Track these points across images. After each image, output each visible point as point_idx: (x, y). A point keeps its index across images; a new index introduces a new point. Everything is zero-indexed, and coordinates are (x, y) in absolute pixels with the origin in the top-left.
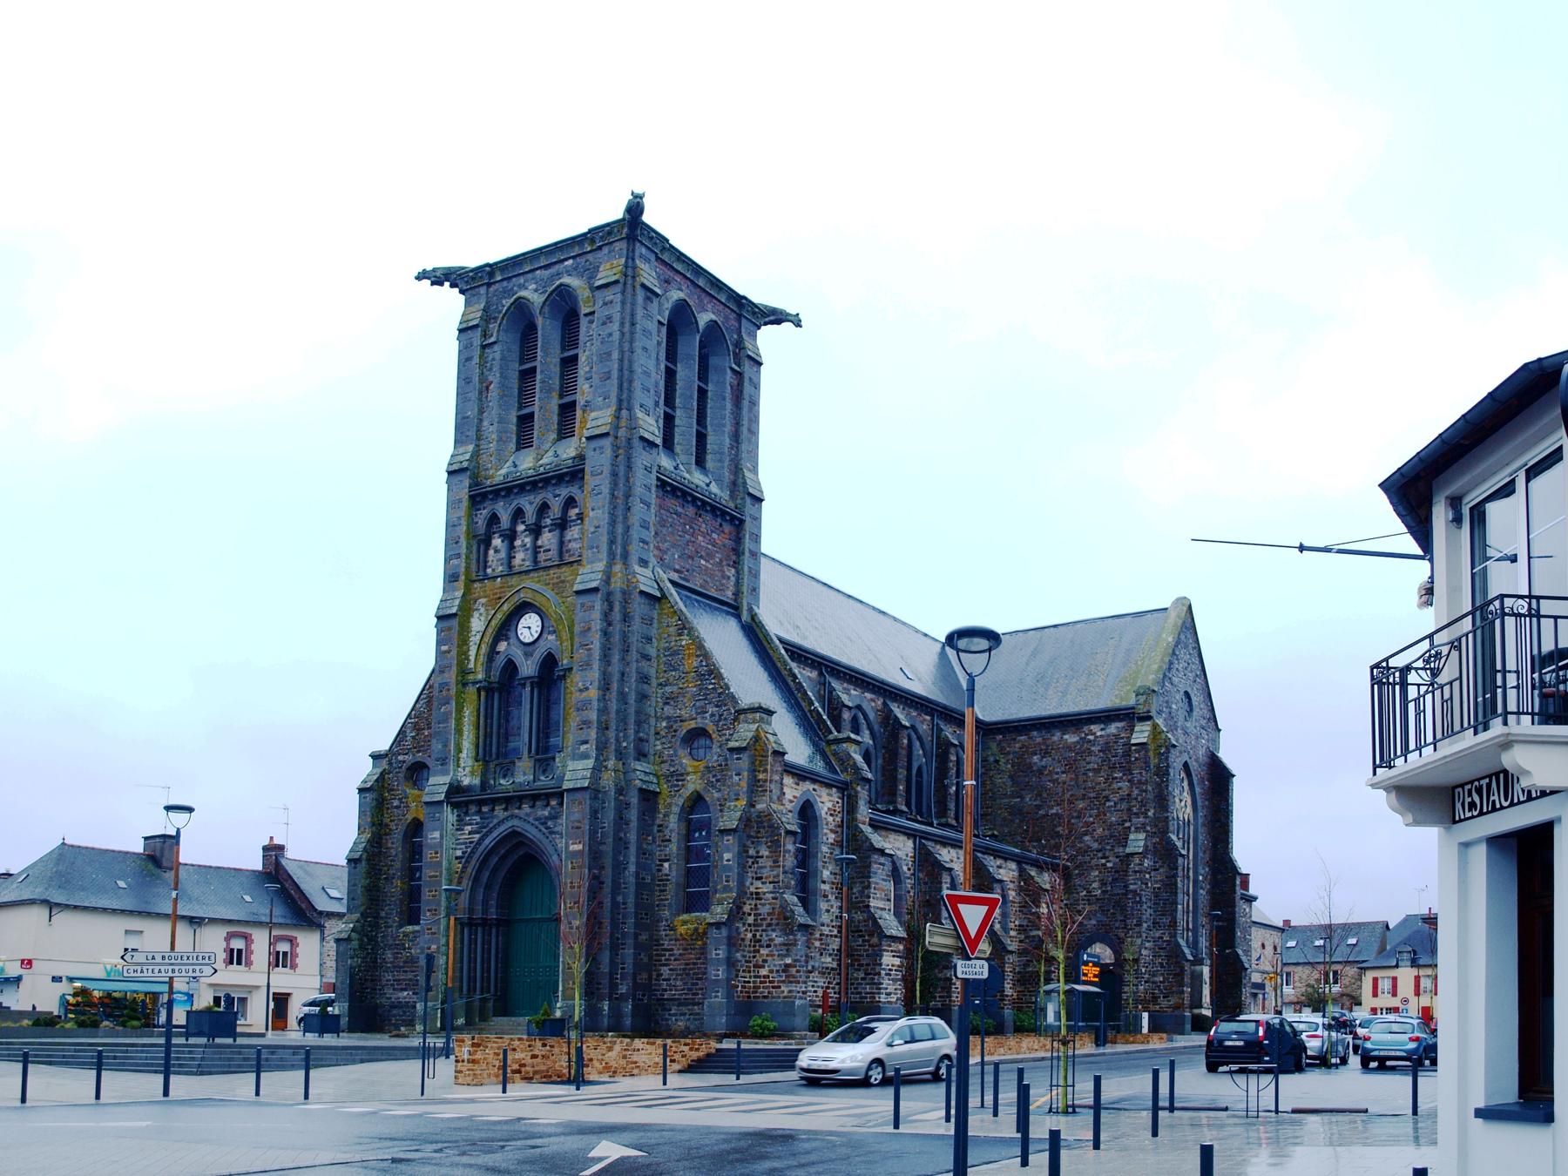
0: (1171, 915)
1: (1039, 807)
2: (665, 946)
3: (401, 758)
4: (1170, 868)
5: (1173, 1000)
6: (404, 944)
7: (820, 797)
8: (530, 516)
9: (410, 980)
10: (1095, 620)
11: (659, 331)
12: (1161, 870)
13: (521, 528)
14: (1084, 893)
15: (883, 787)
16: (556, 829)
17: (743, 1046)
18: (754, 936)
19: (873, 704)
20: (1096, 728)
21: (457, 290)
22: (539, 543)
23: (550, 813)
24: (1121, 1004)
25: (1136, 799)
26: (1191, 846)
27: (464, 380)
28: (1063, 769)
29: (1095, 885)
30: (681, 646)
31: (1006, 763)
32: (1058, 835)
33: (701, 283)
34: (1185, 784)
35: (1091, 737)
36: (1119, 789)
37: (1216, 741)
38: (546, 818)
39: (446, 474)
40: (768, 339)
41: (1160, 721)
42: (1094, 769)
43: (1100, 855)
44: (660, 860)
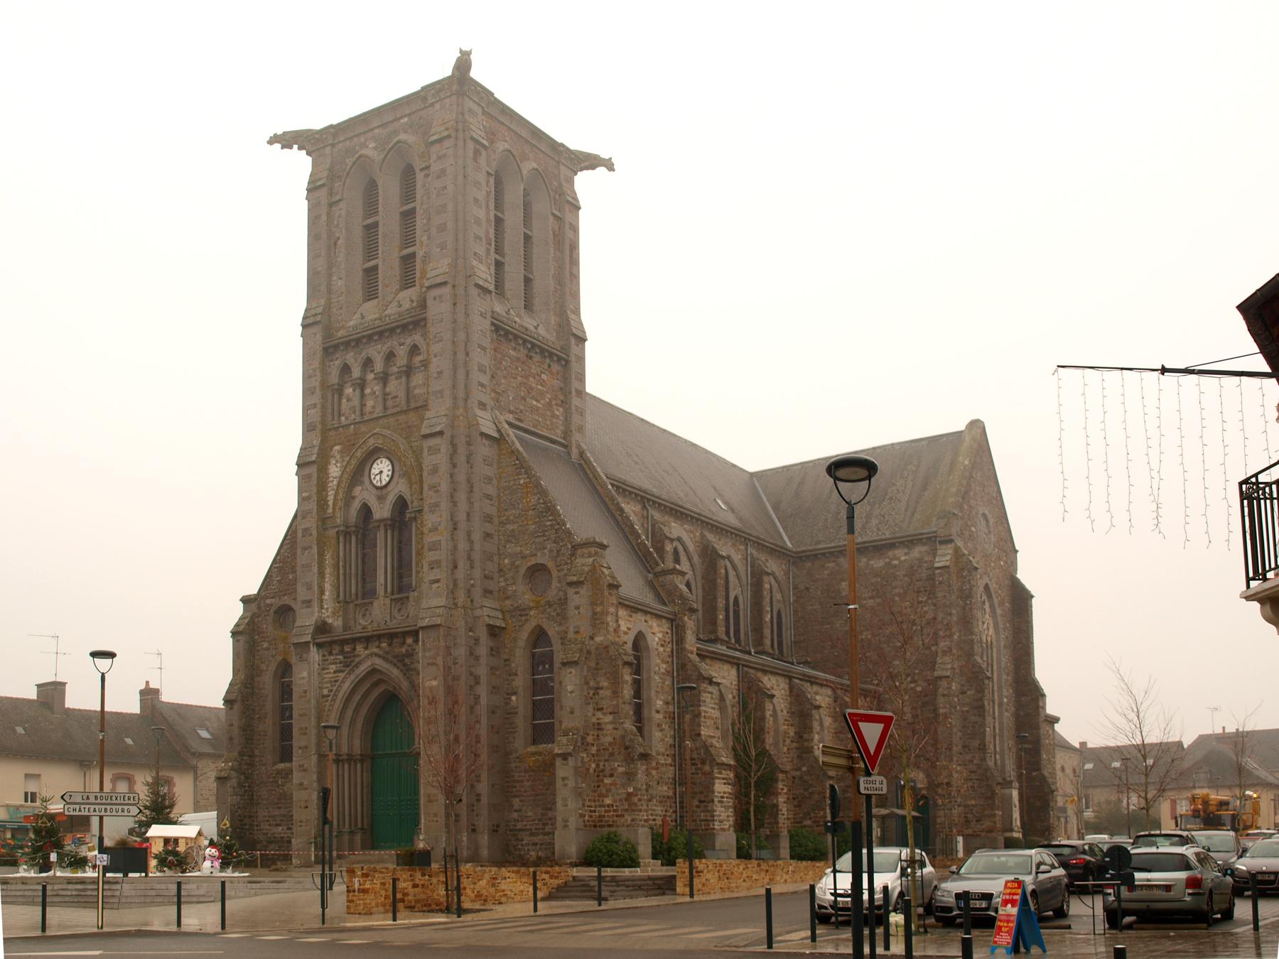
2: (516, 778)
3: (268, 601)
6: (277, 782)
9: (284, 816)
18: (598, 766)
21: (304, 152)
22: (387, 390)
23: (407, 651)
28: (870, 594)
30: (519, 484)
35: (896, 562)
38: (404, 655)
40: (584, 183)
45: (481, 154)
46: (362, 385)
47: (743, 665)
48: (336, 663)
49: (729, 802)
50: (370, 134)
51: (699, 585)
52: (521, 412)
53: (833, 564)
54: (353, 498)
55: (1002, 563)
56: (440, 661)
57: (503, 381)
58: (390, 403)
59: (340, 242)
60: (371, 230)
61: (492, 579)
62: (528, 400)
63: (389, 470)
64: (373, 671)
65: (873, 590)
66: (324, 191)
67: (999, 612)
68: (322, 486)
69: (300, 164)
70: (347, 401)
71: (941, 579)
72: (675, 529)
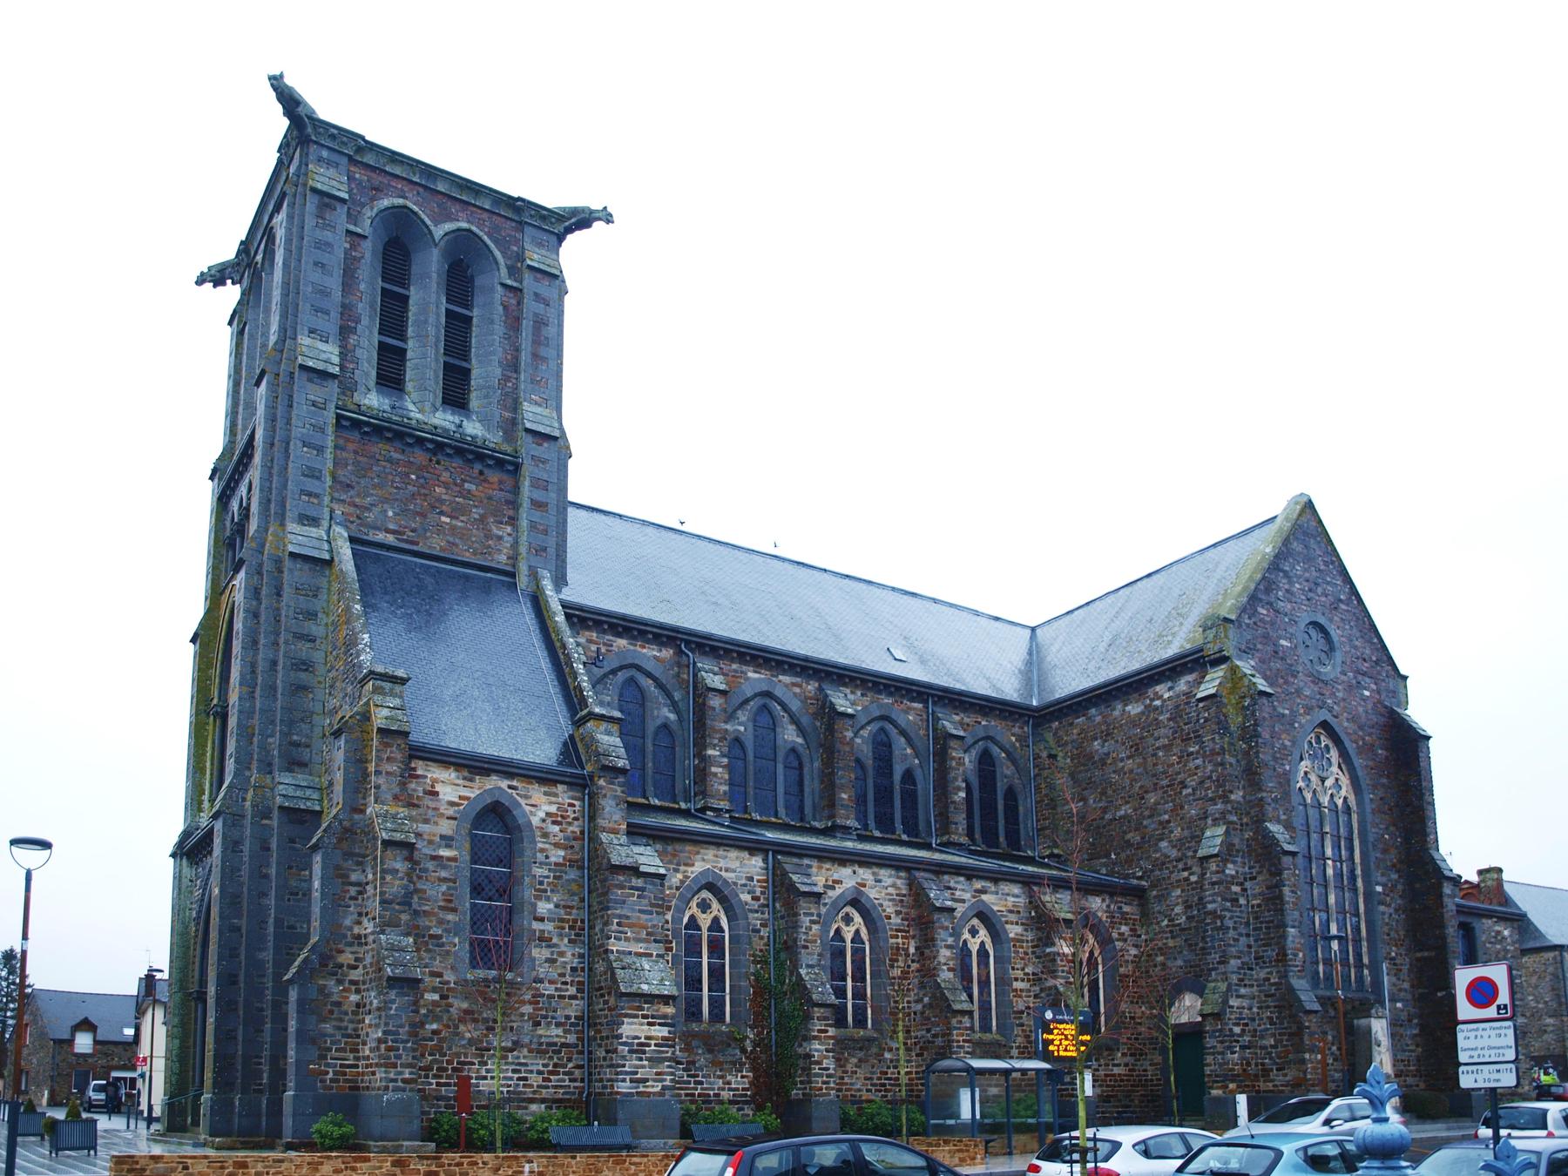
0: (1278, 944)
1: (1105, 810)
4: (1272, 874)
5: (1291, 1074)
7: (526, 797)
10: (1192, 556)
12: (1260, 878)
14: (1166, 922)
15: (821, 798)
19: (797, 690)
20: (1161, 689)
21: (206, 270)
24: (1204, 1083)
25: (1210, 777)
26: (1356, 843)
29: (1178, 909)
31: (1064, 758)
32: (1129, 844)
33: (441, 187)
34: (1334, 755)
35: (1158, 703)
36: (1197, 768)
41: (1246, 666)
42: (1164, 746)
43: (1180, 866)
65: (1132, 747)
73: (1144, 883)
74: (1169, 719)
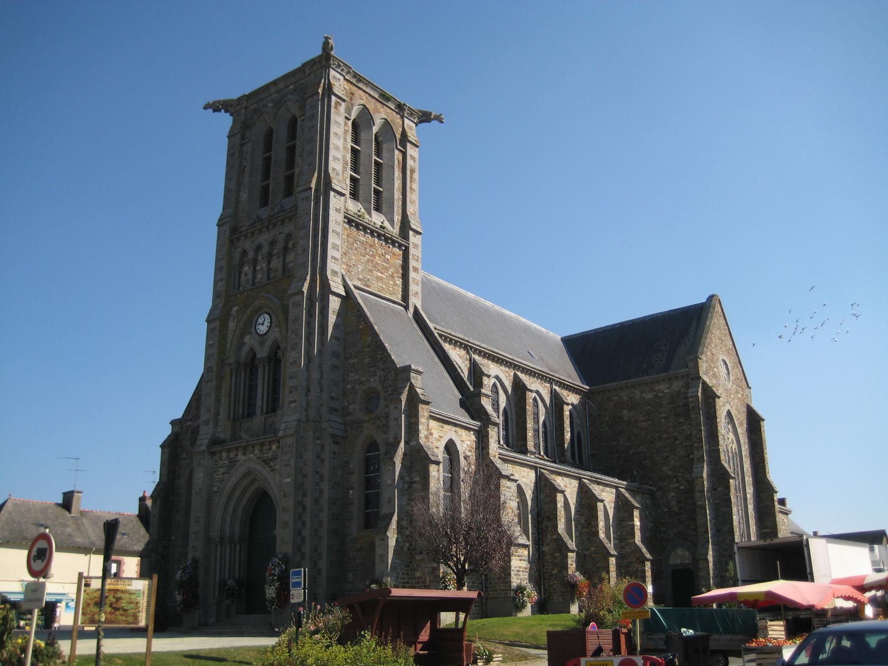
3: (188, 424)
8: (266, 249)
11: (346, 124)
13: (260, 258)
16: (275, 468)
17: (155, 648)
18: (411, 545)
21: (229, 114)
22: (271, 266)
27: (230, 166)
28: (644, 418)
37: (748, 396)
39: (217, 227)
43: (675, 480)
44: (347, 489)
45: (341, 105)
46: (255, 261)
47: (540, 468)
48: (224, 467)
49: (524, 575)
50: (270, 98)
51: (513, 411)
52: (368, 280)
53: (617, 398)
54: (244, 344)
55: (740, 396)
56: (292, 462)
57: (353, 257)
58: (272, 275)
59: (246, 169)
60: (267, 161)
61: (337, 400)
62: (374, 272)
63: (268, 323)
64: (249, 472)
65: (646, 416)
66: (238, 137)
67: (739, 430)
68: (223, 337)
69: (225, 121)
70: (245, 275)
71: (693, 405)
72: (492, 369)
73: (653, 488)
74: (668, 404)
